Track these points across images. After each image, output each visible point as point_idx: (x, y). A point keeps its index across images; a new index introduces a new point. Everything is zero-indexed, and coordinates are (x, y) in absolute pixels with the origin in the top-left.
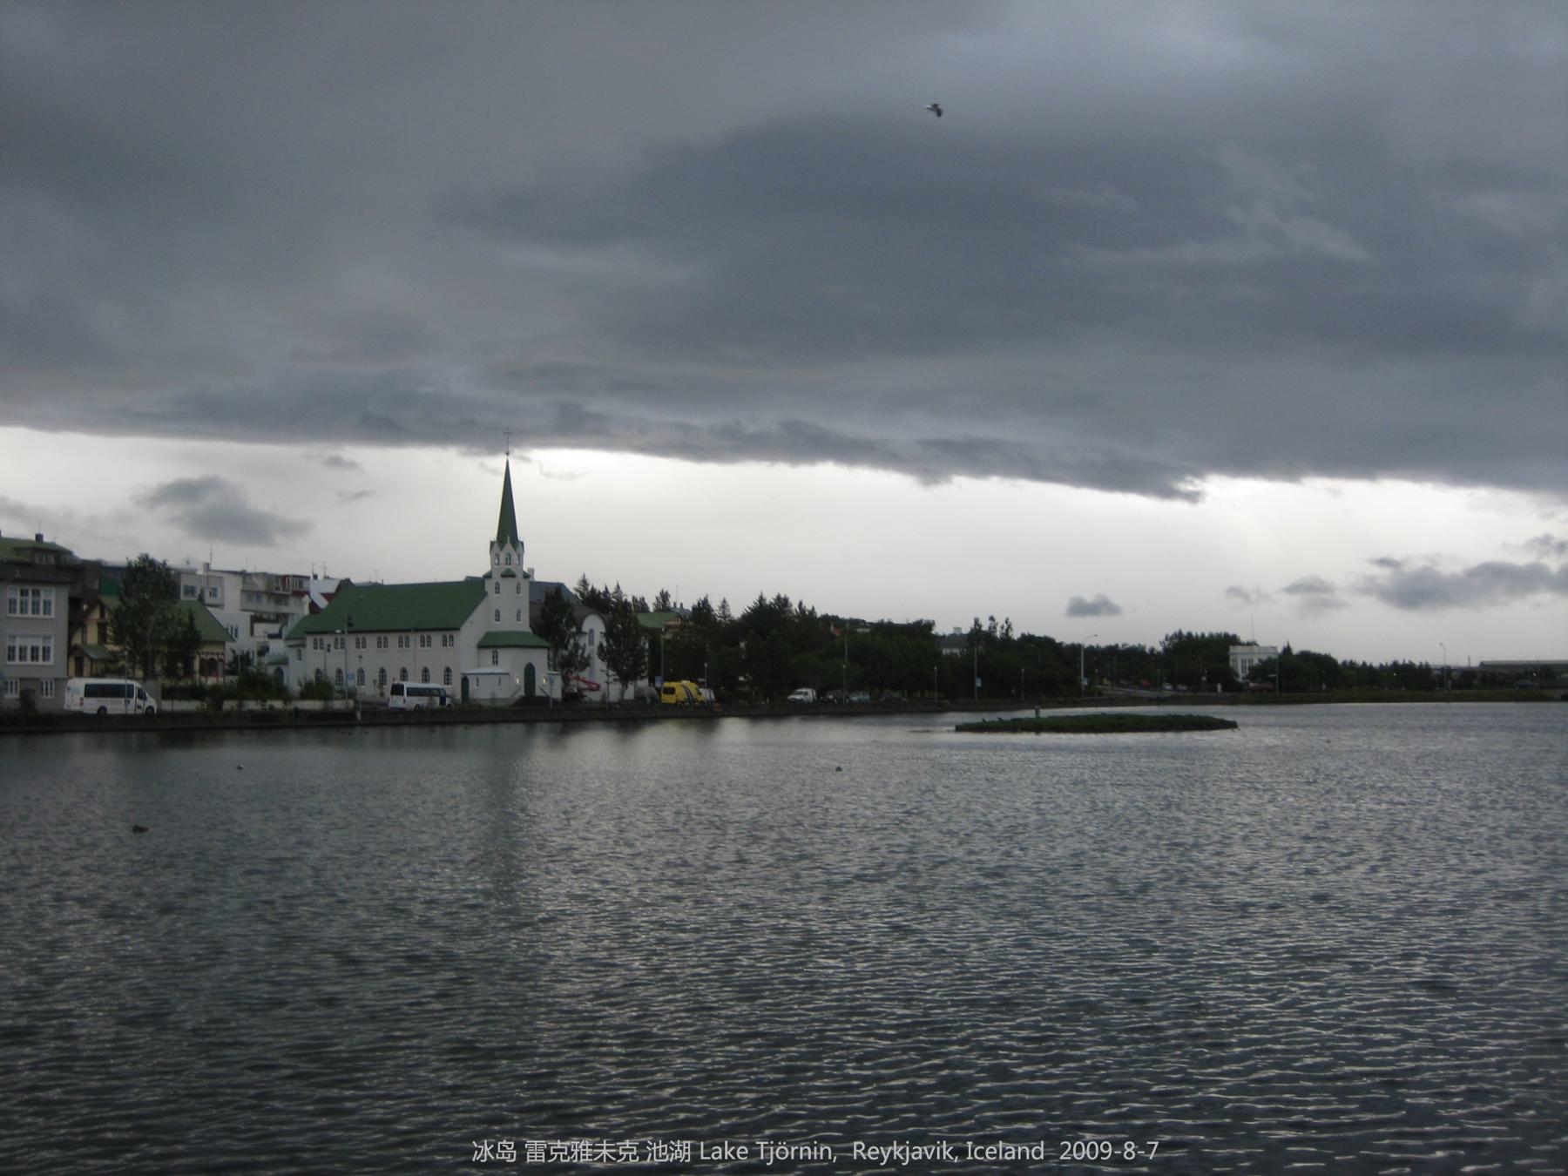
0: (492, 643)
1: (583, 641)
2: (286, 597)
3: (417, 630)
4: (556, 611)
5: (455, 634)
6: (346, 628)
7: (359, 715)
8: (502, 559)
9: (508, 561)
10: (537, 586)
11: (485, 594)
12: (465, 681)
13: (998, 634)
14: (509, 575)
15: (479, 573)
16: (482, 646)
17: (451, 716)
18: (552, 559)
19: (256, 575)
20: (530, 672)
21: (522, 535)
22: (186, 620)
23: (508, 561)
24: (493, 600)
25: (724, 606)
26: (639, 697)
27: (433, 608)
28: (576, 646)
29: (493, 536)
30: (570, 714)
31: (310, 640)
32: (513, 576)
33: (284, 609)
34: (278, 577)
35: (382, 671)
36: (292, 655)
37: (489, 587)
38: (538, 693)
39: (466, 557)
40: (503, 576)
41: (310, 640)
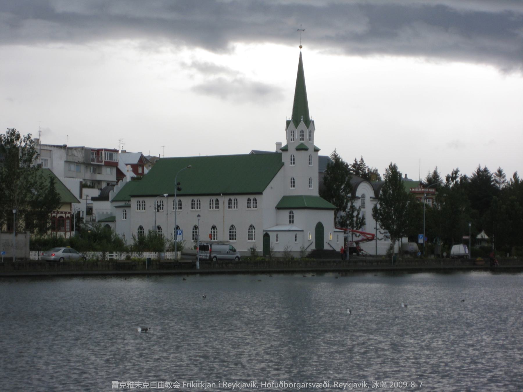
0: (288, 205)
1: (357, 204)
2: (99, 166)
3: (225, 194)
4: (338, 179)
5: (257, 197)
6: (175, 192)
7: (198, 264)
8: (297, 136)
9: (302, 135)
10: (323, 160)
11: (283, 164)
12: (266, 236)
13: (58, 238)
14: (301, 148)
15: (270, 147)
16: (279, 208)
17: (263, 264)
18: (332, 139)
19: (76, 148)
20: (320, 229)
21: (313, 115)
22: (47, 183)
23: (302, 135)
24: (288, 170)
25: (500, 173)
26: (403, 251)
27: (238, 176)
28: (352, 207)
29: (289, 117)
30: (348, 264)
31: (134, 202)
32: (306, 149)
33: (98, 177)
34: (93, 150)
35: (214, 227)
36: (118, 214)
37: (286, 158)
38: (326, 247)
39: (264, 131)
40: (298, 149)
41: (134, 202)
